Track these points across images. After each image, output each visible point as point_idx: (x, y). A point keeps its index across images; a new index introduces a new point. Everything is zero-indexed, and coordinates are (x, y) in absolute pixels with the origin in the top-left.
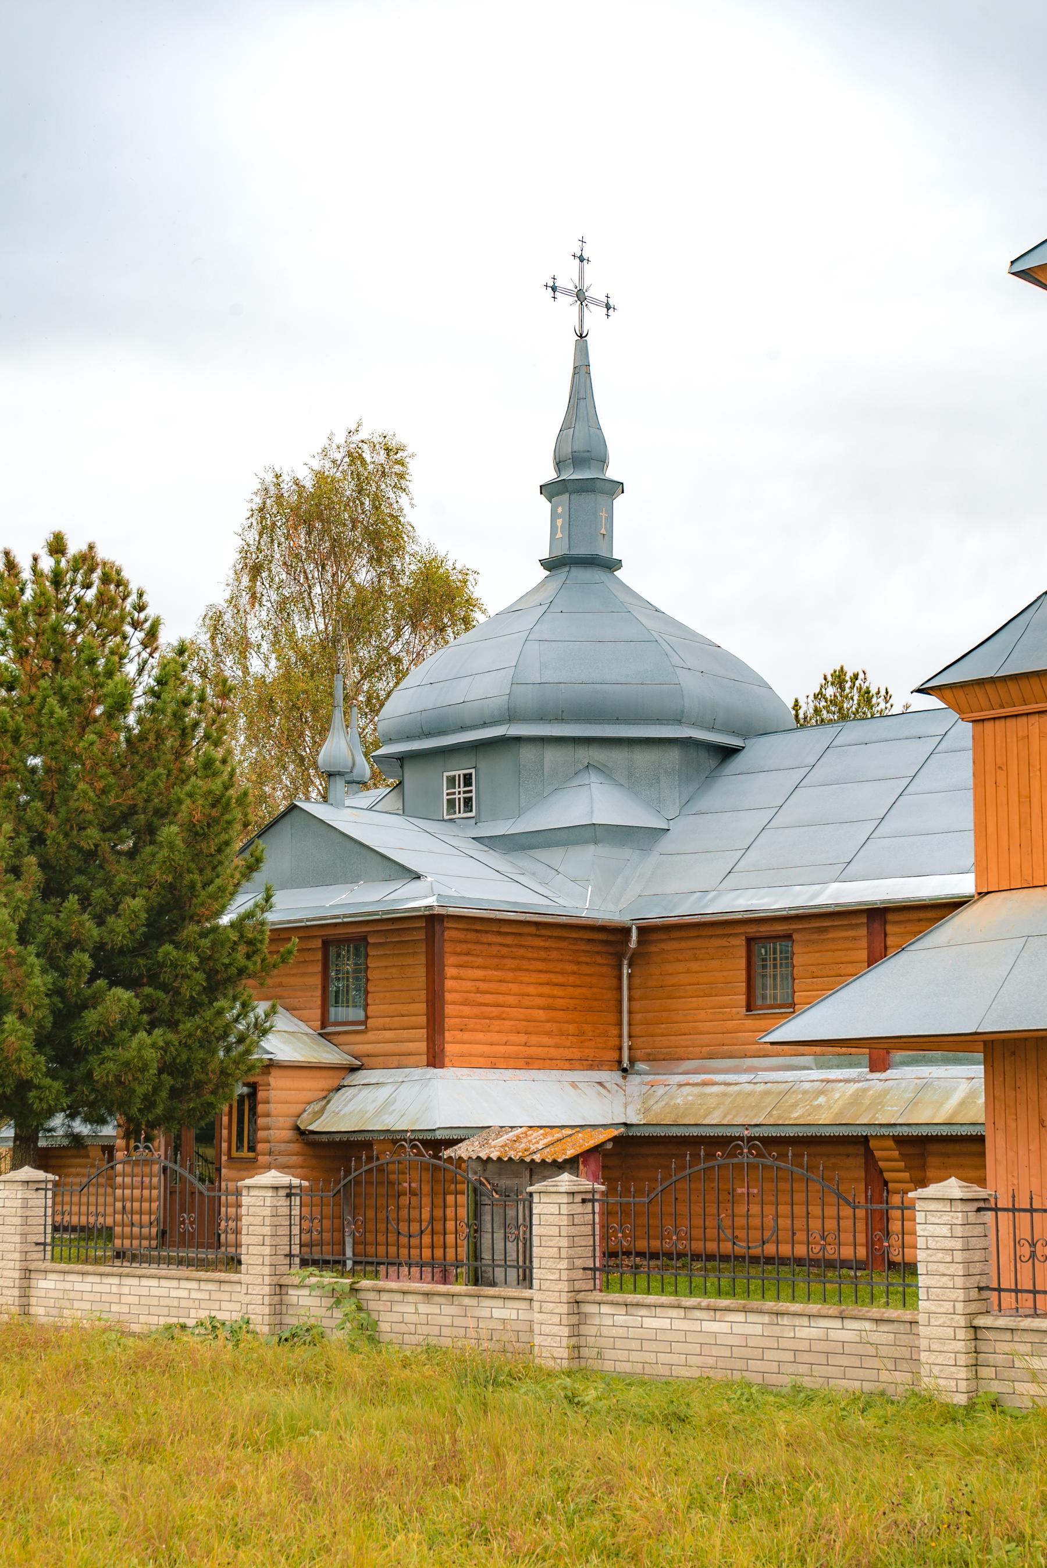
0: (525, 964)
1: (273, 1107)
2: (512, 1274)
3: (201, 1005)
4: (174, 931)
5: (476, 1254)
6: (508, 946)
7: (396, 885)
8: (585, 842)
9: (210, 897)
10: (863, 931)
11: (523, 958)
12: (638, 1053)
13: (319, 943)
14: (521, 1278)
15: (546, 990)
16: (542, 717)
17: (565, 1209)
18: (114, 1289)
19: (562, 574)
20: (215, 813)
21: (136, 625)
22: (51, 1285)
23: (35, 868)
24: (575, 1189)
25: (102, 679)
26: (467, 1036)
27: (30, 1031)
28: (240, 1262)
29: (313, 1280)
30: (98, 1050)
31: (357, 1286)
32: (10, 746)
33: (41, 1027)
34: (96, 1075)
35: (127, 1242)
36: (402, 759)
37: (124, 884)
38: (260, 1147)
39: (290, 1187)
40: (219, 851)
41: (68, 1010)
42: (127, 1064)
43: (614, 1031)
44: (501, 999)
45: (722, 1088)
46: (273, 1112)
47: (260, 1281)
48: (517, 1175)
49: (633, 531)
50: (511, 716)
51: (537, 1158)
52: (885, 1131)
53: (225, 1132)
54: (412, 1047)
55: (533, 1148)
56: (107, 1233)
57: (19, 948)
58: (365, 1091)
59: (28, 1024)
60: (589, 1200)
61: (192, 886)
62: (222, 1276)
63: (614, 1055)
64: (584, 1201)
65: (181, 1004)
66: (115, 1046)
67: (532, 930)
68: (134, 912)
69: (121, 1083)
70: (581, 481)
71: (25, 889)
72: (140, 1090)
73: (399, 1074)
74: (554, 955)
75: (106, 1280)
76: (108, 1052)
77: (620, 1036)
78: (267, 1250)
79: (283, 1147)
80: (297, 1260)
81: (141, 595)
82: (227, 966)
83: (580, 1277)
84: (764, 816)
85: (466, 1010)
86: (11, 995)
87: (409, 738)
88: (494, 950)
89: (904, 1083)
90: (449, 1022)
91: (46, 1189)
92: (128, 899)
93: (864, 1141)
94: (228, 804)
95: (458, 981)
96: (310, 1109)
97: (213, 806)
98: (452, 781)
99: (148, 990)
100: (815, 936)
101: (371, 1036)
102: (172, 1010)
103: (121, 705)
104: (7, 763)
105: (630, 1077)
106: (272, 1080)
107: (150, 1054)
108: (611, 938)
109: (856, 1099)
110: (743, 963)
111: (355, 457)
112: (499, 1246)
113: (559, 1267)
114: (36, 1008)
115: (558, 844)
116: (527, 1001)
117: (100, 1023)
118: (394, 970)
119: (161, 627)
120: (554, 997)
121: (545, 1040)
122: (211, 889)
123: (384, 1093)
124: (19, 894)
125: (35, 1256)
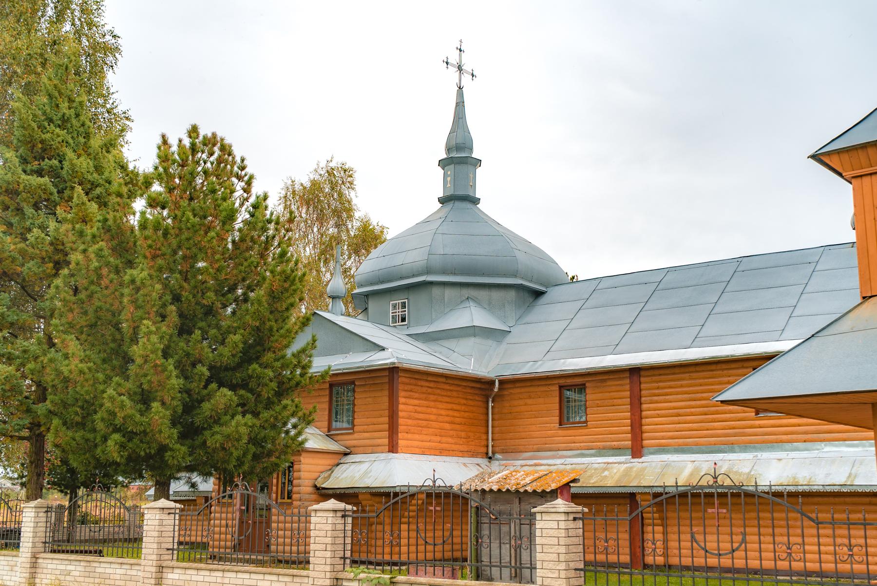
0: (440, 398)
1: (302, 474)
2: (506, 572)
3: (273, 403)
4: (258, 358)
5: (478, 559)
6: (431, 388)
7: (372, 353)
8: (469, 336)
9: (281, 336)
10: (628, 381)
11: (439, 395)
12: (497, 449)
13: (327, 386)
14: (513, 575)
15: (451, 413)
16: (444, 272)
17: (562, 525)
18: (219, 580)
19: (450, 205)
20: (286, 285)
21: (240, 178)
22: (176, 576)
23: (174, 314)
24: (570, 510)
25: (219, 202)
26: (410, 436)
27: (168, 413)
28: (308, 562)
29: (362, 576)
30: (210, 427)
31: (394, 580)
32: (162, 239)
33: (175, 412)
34: (209, 443)
35: (216, 550)
36: (367, 295)
37: (229, 327)
38: (294, 496)
39: (345, 510)
40: (287, 309)
41: (191, 405)
42: (228, 436)
43: (484, 437)
44: (427, 416)
45: (547, 467)
46: (302, 477)
47: (323, 575)
48: (509, 502)
49: (485, 185)
50: (428, 271)
51: (529, 489)
52: (647, 490)
53: (274, 488)
54: (379, 441)
55: (522, 483)
56: (204, 546)
57: (163, 361)
58: (353, 466)
59: (167, 409)
60: (580, 519)
61: (271, 329)
62: (295, 572)
63: (484, 450)
64: (575, 519)
65: (261, 402)
66: (221, 425)
67: (443, 380)
68: (235, 343)
69: (224, 449)
70: (459, 158)
71: (168, 326)
72: (236, 454)
73: (373, 457)
74: (455, 394)
75: (213, 574)
76: (217, 428)
77: (487, 440)
78: (328, 554)
79: (307, 496)
80: (348, 561)
81: (243, 160)
82: (290, 380)
83: (573, 575)
84: (564, 324)
85: (410, 422)
86: (157, 391)
87: (372, 284)
88: (424, 389)
89: (654, 464)
90: (401, 428)
91: (175, 514)
92: (231, 336)
93: (632, 496)
94: (294, 280)
95: (406, 406)
96: (322, 476)
97: (285, 281)
98: (394, 306)
99: (242, 392)
100: (599, 384)
101: (356, 436)
102: (256, 405)
103: (231, 216)
104: (160, 250)
105: (493, 462)
106: (302, 458)
107: (243, 430)
108: (483, 387)
109: (627, 472)
110: (557, 399)
111: (330, 172)
112: (495, 552)
113: (558, 568)
114: (173, 399)
115: (454, 337)
116: (441, 418)
117: (212, 410)
118: (370, 399)
119: (254, 180)
120: (454, 417)
121: (450, 440)
122: (282, 331)
123: (364, 467)
124: (164, 329)
125: (166, 557)
